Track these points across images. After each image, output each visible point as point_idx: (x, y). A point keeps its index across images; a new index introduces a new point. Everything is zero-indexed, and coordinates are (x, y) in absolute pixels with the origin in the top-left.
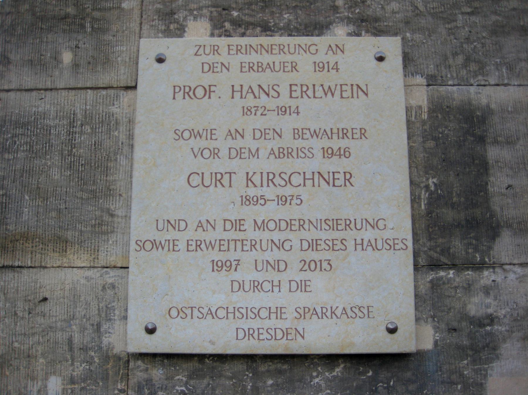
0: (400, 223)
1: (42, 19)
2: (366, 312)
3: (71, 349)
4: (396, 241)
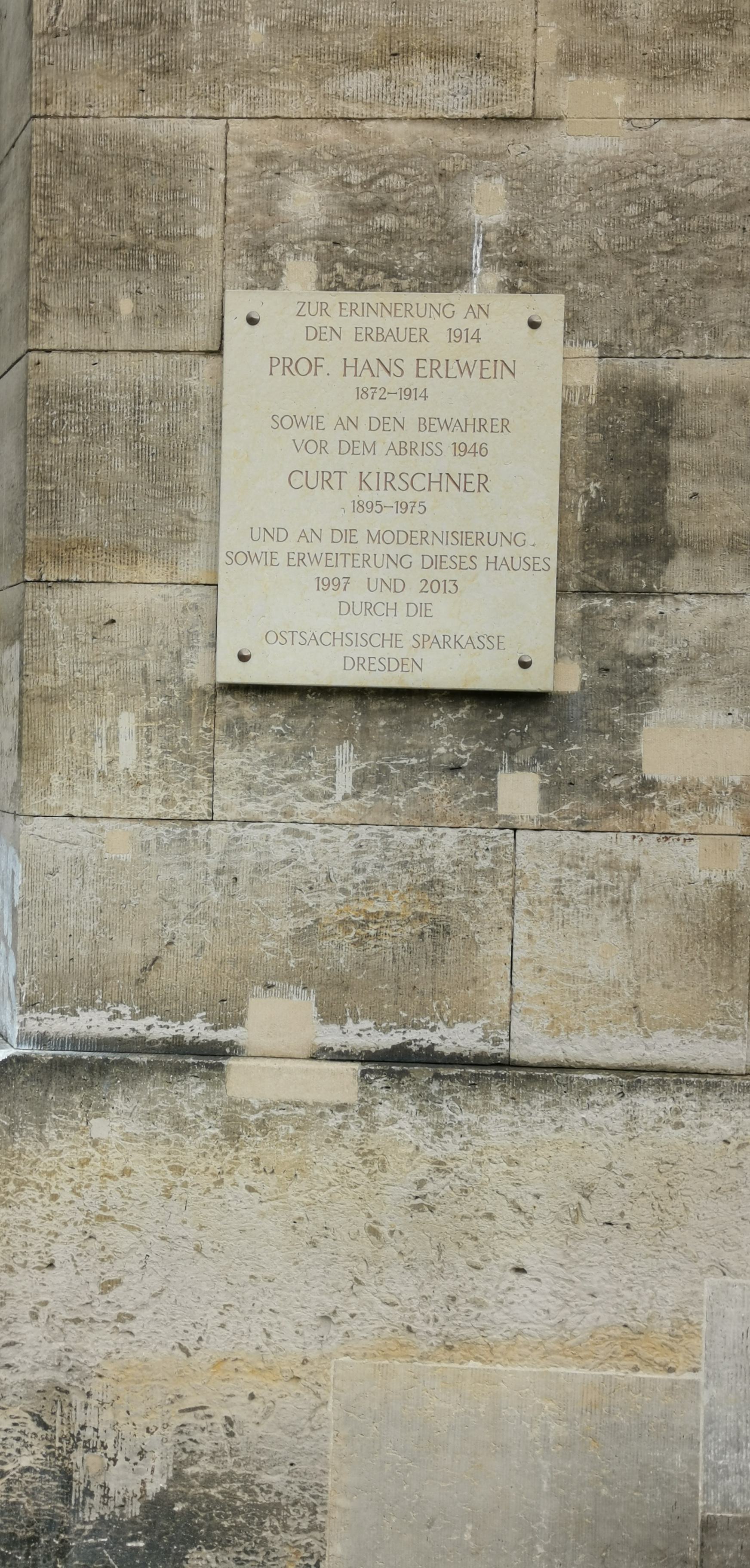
0: (544, 539)
1: (88, 248)
2: (495, 642)
3: (146, 681)
4: (537, 561)
